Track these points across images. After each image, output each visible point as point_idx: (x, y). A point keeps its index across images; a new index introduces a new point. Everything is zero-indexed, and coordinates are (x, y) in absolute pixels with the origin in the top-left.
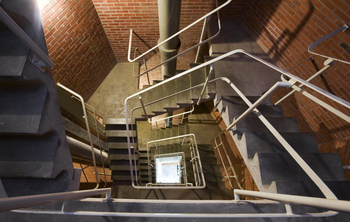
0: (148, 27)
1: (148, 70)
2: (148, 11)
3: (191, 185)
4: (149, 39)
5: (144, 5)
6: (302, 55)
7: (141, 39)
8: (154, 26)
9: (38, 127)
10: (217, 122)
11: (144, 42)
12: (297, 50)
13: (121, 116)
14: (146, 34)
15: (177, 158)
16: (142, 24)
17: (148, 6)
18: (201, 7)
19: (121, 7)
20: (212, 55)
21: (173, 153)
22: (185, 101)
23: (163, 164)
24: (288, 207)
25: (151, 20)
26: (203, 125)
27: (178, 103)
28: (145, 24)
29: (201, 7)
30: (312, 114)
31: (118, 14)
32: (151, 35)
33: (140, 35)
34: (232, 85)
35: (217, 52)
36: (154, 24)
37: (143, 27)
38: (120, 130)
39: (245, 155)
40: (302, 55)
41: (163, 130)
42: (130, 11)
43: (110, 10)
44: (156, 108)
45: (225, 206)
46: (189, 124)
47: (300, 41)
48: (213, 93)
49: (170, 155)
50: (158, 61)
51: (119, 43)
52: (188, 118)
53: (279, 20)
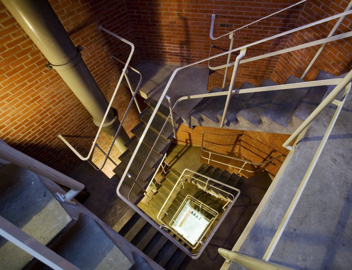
0: (73, 120)
1: (107, 153)
2: (64, 108)
3: (213, 219)
4: (82, 130)
5: (57, 105)
6: (204, 49)
7: (74, 136)
8: (78, 115)
9: (126, 258)
10: (188, 145)
11: (78, 136)
12: (198, 48)
13: (119, 216)
14: (76, 128)
15: (186, 208)
16: (65, 122)
17: (60, 103)
18: (106, 72)
19: (34, 123)
20: (148, 96)
21: (180, 206)
22: (163, 145)
23: (180, 226)
24: (336, 102)
25: (72, 112)
26: (182, 158)
27: (159, 152)
28: (69, 120)
29: (106, 72)
30: (243, 76)
31: (79, 105)
32: (81, 125)
33: (70, 133)
34: (192, 97)
35: (149, 91)
36: (77, 114)
37: (69, 124)
38: (130, 229)
39: (253, 128)
40: (204, 49)
41: (156, 195)
42: (46, 120)
43: (24, 135)
44: (144, 176)
45: (295, 158)
46: (173, 168)
47: (195, 42)
48: (179, 119)
49: (180, 209)
50: (104, 141)
51: (55, 157)
52: (166, 165)
53: (170, 40)
